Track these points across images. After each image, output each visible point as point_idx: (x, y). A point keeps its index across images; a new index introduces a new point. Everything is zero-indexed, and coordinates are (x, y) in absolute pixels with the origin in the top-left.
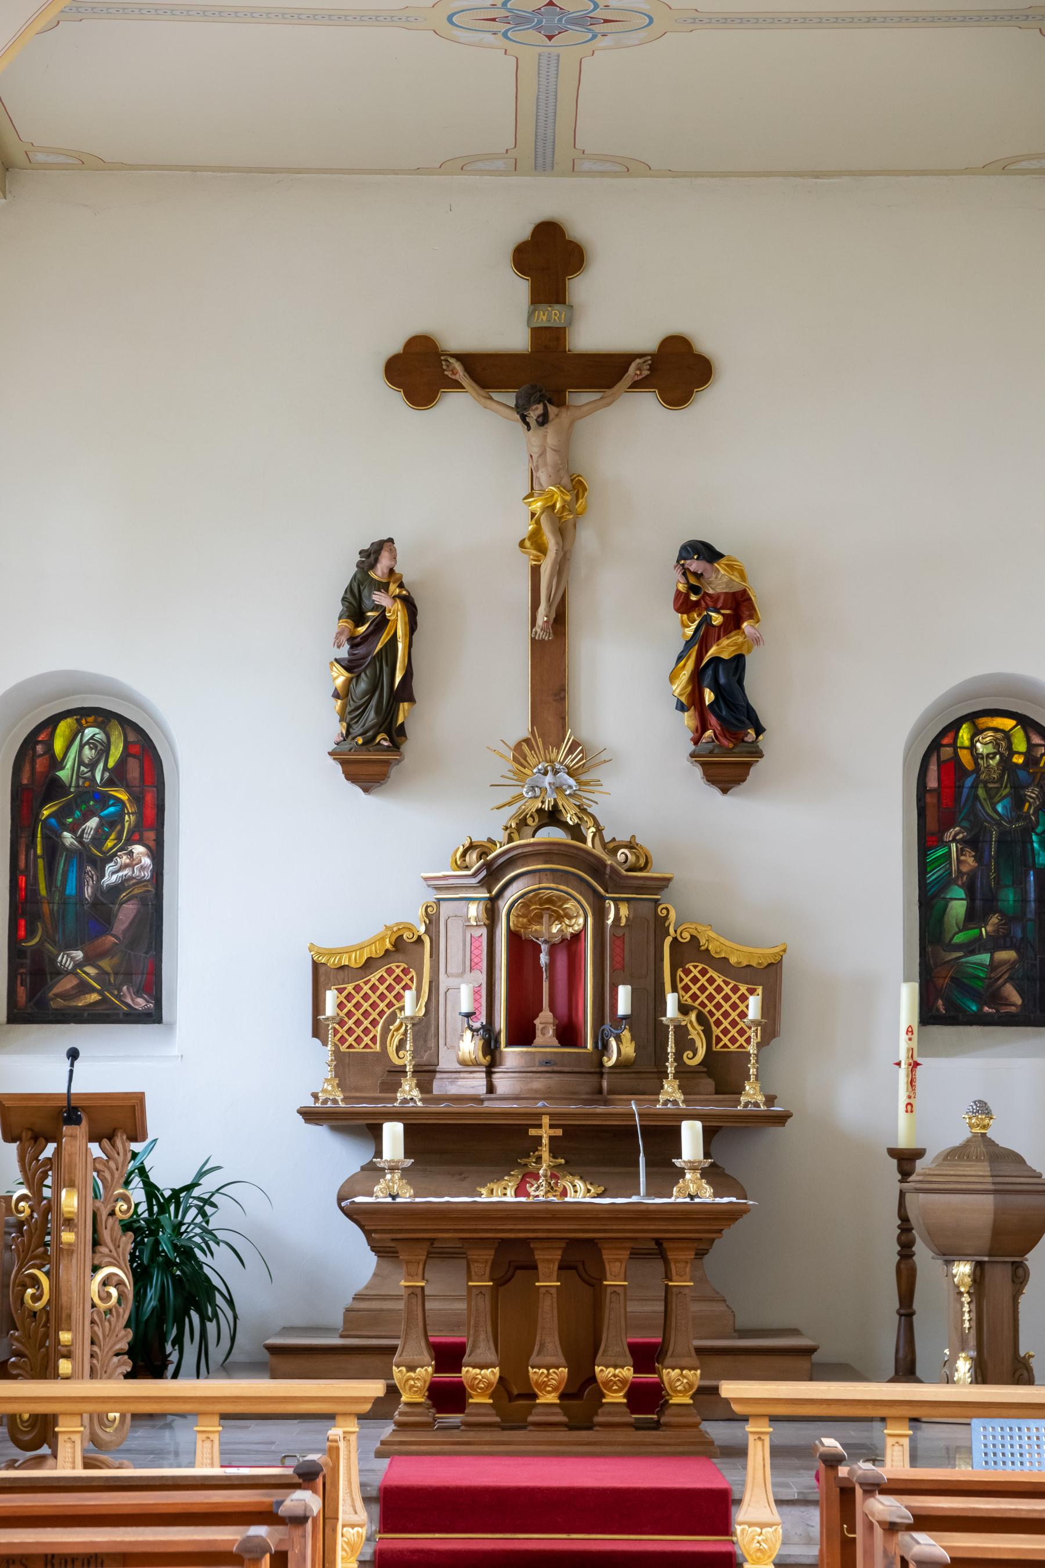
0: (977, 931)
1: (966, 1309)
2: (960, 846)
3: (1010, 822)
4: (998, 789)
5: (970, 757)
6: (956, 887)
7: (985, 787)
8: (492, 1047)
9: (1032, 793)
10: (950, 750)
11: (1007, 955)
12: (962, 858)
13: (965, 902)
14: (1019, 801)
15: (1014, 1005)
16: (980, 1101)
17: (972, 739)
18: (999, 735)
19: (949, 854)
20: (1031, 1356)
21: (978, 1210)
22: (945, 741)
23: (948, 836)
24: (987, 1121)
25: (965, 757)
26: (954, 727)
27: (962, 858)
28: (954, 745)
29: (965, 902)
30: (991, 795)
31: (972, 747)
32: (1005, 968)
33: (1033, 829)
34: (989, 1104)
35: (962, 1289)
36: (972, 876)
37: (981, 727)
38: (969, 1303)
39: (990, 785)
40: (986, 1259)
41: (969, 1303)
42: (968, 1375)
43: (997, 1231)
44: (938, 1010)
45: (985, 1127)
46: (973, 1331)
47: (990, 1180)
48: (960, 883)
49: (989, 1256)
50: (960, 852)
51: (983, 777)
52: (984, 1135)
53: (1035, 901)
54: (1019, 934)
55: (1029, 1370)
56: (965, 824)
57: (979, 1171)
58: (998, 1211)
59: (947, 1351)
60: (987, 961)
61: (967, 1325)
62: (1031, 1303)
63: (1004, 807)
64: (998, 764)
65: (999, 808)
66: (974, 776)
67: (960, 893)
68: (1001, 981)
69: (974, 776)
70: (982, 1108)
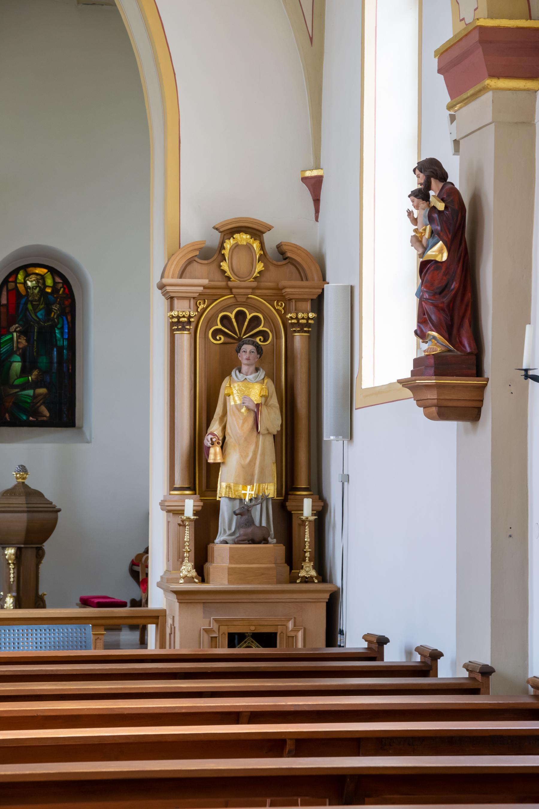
0: (26, 378)
1: (12, 572)
2: (18, 334)
3: (44, 322)
4: (38, 305)
5: (23, 288)
6: (16, 356)
7: (32, 304)
8: (245, 390)
9: (55, 307)
10: (13, 284)
11: (42, 391)
12: (19, 340)
13: (20, 363)
14: (49, 311)
15: (45, 416)
16: (22, 466)
17: (24, 279)
18: (39, 277)
19: (13, 338)
20: (45, 595)
21: (19, 521)
22: (11, 279)
23: (12, 328)
24: (25, 475)
25: (21, 287)
26: (15, 272)
27: (19, 340)
28: (15, 282)
29: (20, 363)
30: (35, 308)
31: (25, 283)
32: (41, 397)
33: (56, 326)
34: (27, 467)
35: (10, 562)
36: (24, 349)
37: (30, 272)
38: (13, 569)
39: (34, 303)
40: (22, 546)
41: (13, 569)
42: (11, 605)
43: (29, 531)
44: (6, 419)
45: (24, 479)
46: (15, 583)
47: (25, 505)
48: (18, 353)
49: (24, 544)
50: (18, 337)
51: (30, 298)
52: (23, 483)
53: (57, 363)
54: (48, 380)
55: (43, 601)
56: (21, 323)
57: (20, 501)
58: (29, 521)
59: (2, 593)
60: (32, 394)
61: (12, 580)
62: (46, 568)
63: (41, 314)
64: (38, 292)
65: (39, 314)
66: (26, 298)
67: (18, 358)
68: (39, 404)
69: (26, 298)
70: (23, 469)
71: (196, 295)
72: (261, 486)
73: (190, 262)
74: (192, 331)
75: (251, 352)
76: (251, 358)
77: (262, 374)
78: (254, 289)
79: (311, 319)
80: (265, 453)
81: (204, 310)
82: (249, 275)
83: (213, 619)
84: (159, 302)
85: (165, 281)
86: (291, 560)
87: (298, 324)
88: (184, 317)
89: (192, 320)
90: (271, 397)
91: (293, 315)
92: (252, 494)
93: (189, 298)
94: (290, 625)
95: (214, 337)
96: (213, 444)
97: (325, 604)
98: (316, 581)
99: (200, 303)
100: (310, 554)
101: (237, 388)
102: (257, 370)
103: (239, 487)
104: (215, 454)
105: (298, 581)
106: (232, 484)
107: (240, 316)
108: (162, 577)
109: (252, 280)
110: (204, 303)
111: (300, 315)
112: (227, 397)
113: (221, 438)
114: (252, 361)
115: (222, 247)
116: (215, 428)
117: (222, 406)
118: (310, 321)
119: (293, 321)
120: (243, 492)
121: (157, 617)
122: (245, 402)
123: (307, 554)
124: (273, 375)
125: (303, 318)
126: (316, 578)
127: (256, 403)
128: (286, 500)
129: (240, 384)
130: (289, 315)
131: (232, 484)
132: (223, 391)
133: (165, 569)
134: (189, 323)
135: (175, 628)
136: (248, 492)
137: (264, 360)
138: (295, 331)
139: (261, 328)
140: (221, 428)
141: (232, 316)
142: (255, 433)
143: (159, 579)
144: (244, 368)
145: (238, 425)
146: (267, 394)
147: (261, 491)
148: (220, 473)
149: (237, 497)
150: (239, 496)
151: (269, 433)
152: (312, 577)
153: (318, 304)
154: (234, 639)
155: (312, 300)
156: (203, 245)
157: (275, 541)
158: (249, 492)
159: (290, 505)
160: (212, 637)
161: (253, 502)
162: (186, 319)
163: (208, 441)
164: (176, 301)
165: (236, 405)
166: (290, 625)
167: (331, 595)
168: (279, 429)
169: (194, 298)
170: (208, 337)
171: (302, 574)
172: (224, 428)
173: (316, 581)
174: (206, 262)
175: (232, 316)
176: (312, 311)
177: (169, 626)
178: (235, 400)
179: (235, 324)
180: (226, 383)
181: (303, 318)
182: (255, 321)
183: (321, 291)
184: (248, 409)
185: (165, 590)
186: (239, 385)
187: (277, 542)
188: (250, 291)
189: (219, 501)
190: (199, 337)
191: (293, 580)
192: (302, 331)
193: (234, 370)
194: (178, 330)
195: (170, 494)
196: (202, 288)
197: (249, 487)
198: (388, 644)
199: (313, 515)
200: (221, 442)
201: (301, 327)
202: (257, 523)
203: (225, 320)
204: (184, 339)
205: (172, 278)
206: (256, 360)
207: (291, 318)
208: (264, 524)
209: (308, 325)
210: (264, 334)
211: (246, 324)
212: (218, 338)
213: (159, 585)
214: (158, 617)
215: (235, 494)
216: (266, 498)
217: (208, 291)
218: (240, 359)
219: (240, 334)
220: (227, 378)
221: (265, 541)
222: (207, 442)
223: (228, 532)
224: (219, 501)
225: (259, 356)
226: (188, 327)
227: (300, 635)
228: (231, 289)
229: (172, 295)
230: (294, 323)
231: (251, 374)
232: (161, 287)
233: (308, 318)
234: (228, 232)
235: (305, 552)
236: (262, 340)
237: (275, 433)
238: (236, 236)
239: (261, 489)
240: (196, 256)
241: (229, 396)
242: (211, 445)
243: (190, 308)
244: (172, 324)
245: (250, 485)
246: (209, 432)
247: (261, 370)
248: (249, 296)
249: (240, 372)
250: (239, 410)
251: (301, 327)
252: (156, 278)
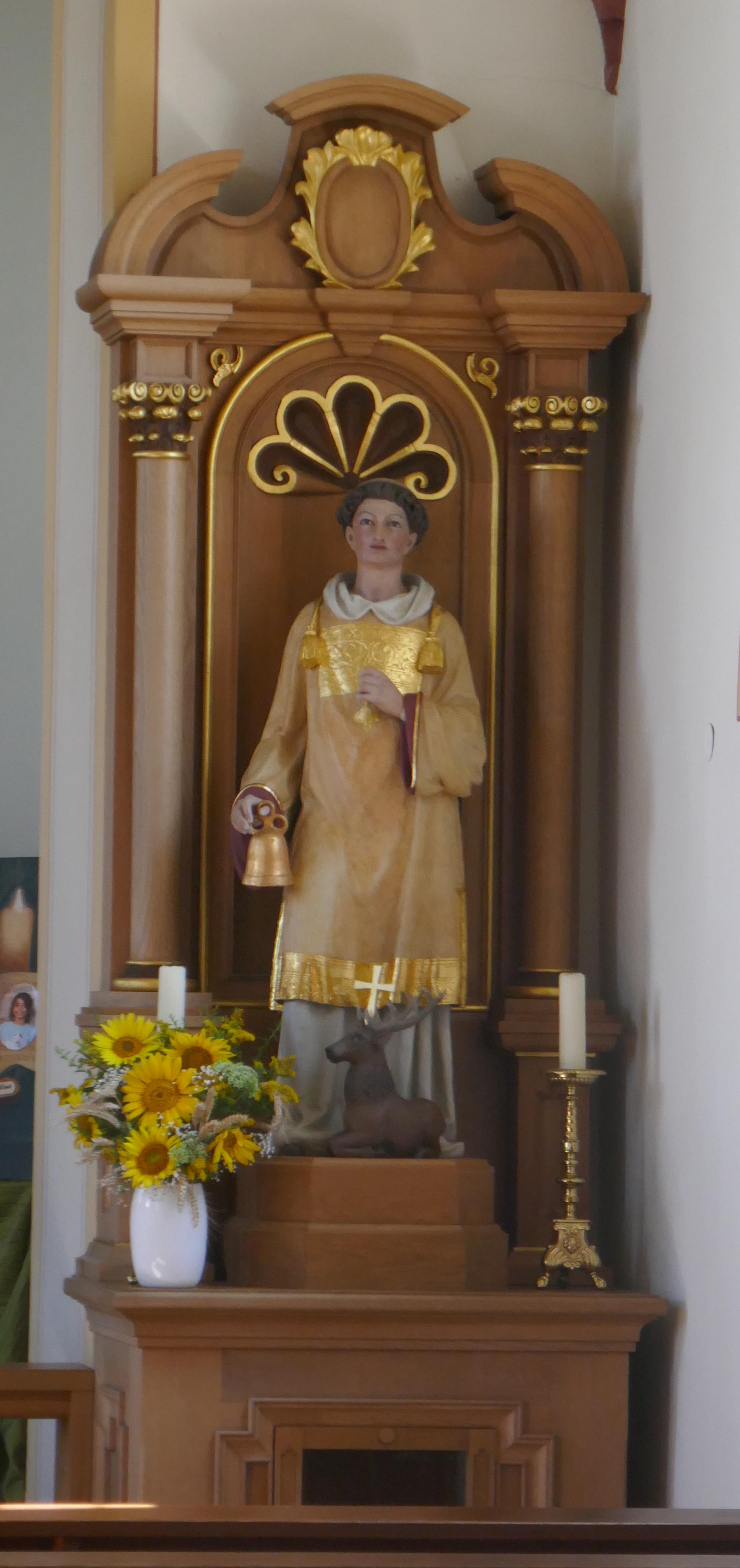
8: (377, 646)
71: (208, 331)
73: (189, 221)
74: (194, 452)
75: (391, 524)
76: (388, 544)
77: (424, 596)
78: (397, 312)
80: (429, 857)
81: (234, 381)
82: (385, 269)
83: (256, 1403)
84: (81, 351)
85: (107, 282)
86: (516, 1210)
87: (546, 434)
88: (167, 403)
89: (195, 413)
90: (454, 677)
91: (530, 404)
92: (386, 993)
93: (186, 342)
94: (511, 1427)
95: (267, 474)
96: (259, 826)
97: (625, 1361)
98: (601, 1283)
99: (220, 357)
100: (579, 1194)
101: (340, 643)
103: (344, 967)
105: (542, 1283)
106: (322, 960)
107: (354, 404)
108: (81, 1262)
109: (393, 283)
110: (234, 359)
112: (309, 673)
113: (286, 807)
115: (297, 174)
116: (267, 772)
118: (586, 426)
119: (530, 424)
120: (359, 985)
121: (65, 1395)
122: (368, 688)
123: (571, 1194)
124: (457, 601)
125: (563, 415)
126: (600, 1272)
127: (403, 691)
128: (496, 1012)
129: (353, 629)
130: (517, 405)
131: (322, 960)
132: (294, 652)
133: (93, 1234)
134: (184, 423)
135: (126, 1430)
137: (436, 559)
138: (535, 458)
139: (420, 445)
140: (285, 774)
141: (327, 403)
142: (401, 791)
143: (71, 1270)
144: (368, 576)
145: (342, 766)
146: (441, 665)
147: (417, 983)
148: (281, 922)
149: (339, 1002)
150: (346, 998)
151: (446, 793)
152: (585, 1269)
153: (613, 364)
154: (332, 1473)
155: (592, 353)
156: (235, 167)
157: (460, 1147)
158: (377, 987)
159: (511, 1029)
160: (250, 1465)
161: (392, 1020)
162: (172, 412)
164: (142, 351)
165: (337, 698)
166: (511, 1427)
167: (646, 1332)
168: (479, 779)
169: (201, 340)
170: (246, 472)
171: (555, 1257)
172: (297, 775)
173: (601, 1283)
174: (240, 221)
175: (327, 403)
176: (593, 392)
177: (106, 1423)
178: (336, 679)
179: (335, 430)
180: (304, 624)
181: (563, 415)
182: (403, 422)
183: (622, 323)
184: (378, 712)
185: (92, 1307)
186: (347, 632)
187: (469, 1153)
188: (386, 320)
191: (522, 1279)
192: (558, 457)
193: (333, 583)
194: (147, 445)
195: (114, 989)
196: (228, 309)
197: (377, 970)
198: (79, 1012)
199: (591, 1064)
200: (285, 818)
201: (557, 444)
202: (405, 1091)
203: (304, 418)
204: (166, 474)
205: (130, 272)
206: (406, 550)
207: (524, 414)
208: (427, 1091)
209: (577, 437)
211: (372, 429)
212: (280, 479)
213: (72, 1288)
214: (66, 1395)
215: (330, 990)
216: (431, 1006)
217: (244, 317)
218: (353, 545)
219: (352, 464)
220: (308, 613)
221: (433, 1150)
222: (242, 815)
223: (311, 1116)
225: (414, 537)
226: (181, 437)
227: (542, 1459)
228: (323, 315)
229: (130, 328)
231: (390, 596)
232: (93, 301)
233: (580, 415)
234: (318, 123)
235: (565, 1187)
236: (424, 483)
237: (466, 792)
238: (344, 136)
239: (417, 975)
240: (208, 201)
241: (316, 666)
242: (253, 831)
243: (188, 373)
244: (129, 426)
245: (380, 962)
246: (245, 784)
247: (423, 584)
248: (384, 337)
250: (348, 714)
251: (557, 444)
252: (75, 275)
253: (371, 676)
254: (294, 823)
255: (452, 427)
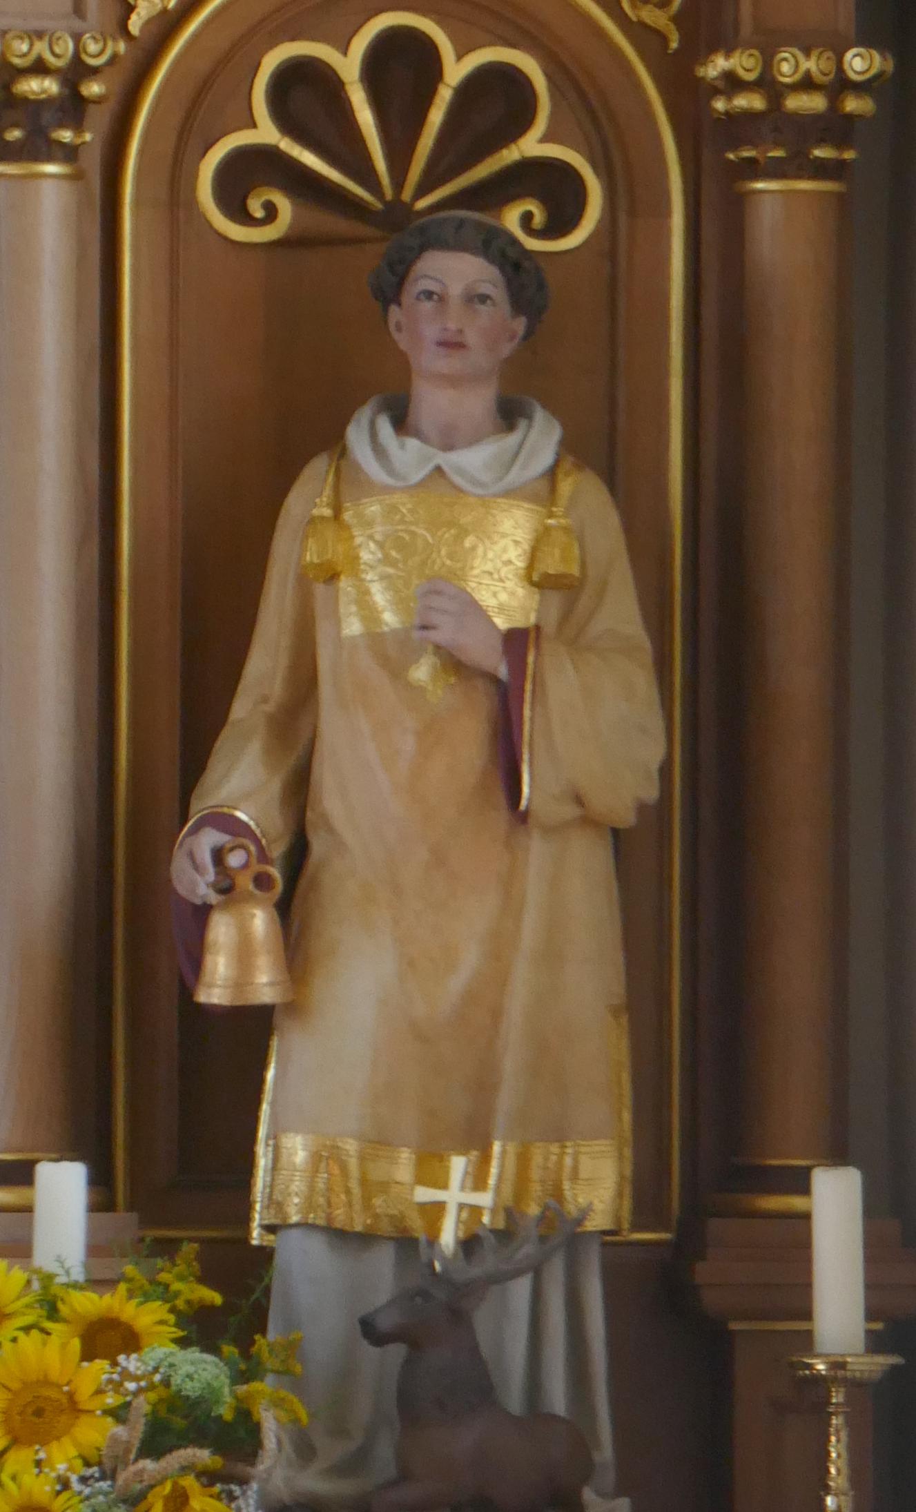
72: (537, 1159)
74: (93, 163)
75: (475, 299)
77: (542, 438)
79: (859, 88)
87: (775, 120)
88: (39, 68)
89: (93, 89)
91: (744, 63)
92: (476, 1210)
96: (226, 888)
101: (379, 531)
102: (509, 414)
103: (393, 1161)
104: (244, 954)
111: (788, 67)
112: (320, 589)
113: (277, 851)
114: (479, 356)
116: (241, 782)
117: (285, 641)
118: (852, 104)
120: (424, 1194)
122: (435, 619)
124: (605, 448)
125: (807, 84)
127: (502, 623)
128: (689, 1243)
129: (405, 504)
130: (717, 65)
131: (351, 1146)
132: (289, 552)
134: (73, 107)
136: (454, 1195)
137: (562, 364)
138: (753, 169)
139: (531, 145)
140: (275, 787)
141: (349, 66)
142: (500, 817)
144: (432, 401)
145: (384, 772)
147: (536, 1189)
148: (270, 1075)
149: (385, 1228)
150: (398, 1221)
151: (588, 821)
158: (459, 1197)
159: (718, 1276)
161: (488, 1262)
163: (197, 867)
168: (651, 793)
170: (193, 202)
175: (349, 66)
176: (866, 39)
178: (372, 601)
179: (365, 117)
181: (807, 84)
184: (454, 665)
186: (392, 509)
189: (265, 1255)
190: (137, 202)
193: (364, 415)
199: (875, 1343)
200: (275, 872)
203: (306, 96)
206: (507, 349)
207: (732, 83)
208: (557, 1399)
209: (835, 127)
210: (557, 191)
212: (259, 214)
215: (367, 1205)
216: (562, 1233)
220: (318, 471)
222: (192, 870)
224: (265, 1255)
226: (66, 136)
230: (749, 116)
231: (474, 440)
233: (841, 85)
236: (539, 219)
237: (626, 818)
239: (535, 1174)
241: (332, 577)
242: (213, 898)
245: (463, 1150)
246: (200, 806)
247: (540, 415)
249: (401, 424)
250: (396, 669)
253: (440, 595)
254: (292, 879)
255: (594, 110)
